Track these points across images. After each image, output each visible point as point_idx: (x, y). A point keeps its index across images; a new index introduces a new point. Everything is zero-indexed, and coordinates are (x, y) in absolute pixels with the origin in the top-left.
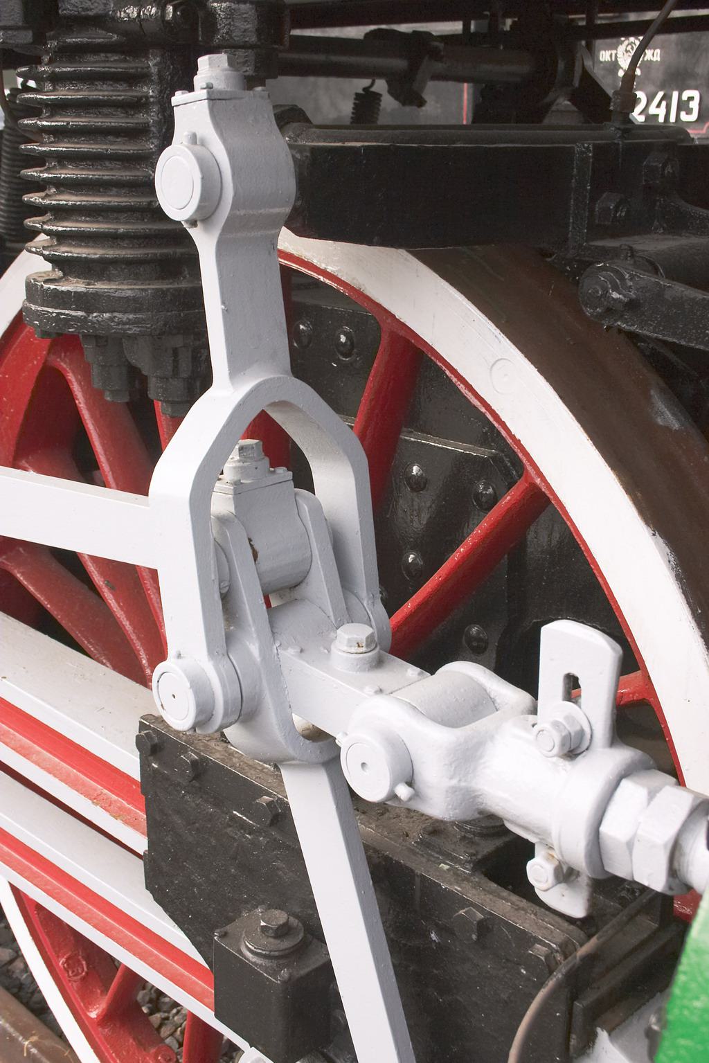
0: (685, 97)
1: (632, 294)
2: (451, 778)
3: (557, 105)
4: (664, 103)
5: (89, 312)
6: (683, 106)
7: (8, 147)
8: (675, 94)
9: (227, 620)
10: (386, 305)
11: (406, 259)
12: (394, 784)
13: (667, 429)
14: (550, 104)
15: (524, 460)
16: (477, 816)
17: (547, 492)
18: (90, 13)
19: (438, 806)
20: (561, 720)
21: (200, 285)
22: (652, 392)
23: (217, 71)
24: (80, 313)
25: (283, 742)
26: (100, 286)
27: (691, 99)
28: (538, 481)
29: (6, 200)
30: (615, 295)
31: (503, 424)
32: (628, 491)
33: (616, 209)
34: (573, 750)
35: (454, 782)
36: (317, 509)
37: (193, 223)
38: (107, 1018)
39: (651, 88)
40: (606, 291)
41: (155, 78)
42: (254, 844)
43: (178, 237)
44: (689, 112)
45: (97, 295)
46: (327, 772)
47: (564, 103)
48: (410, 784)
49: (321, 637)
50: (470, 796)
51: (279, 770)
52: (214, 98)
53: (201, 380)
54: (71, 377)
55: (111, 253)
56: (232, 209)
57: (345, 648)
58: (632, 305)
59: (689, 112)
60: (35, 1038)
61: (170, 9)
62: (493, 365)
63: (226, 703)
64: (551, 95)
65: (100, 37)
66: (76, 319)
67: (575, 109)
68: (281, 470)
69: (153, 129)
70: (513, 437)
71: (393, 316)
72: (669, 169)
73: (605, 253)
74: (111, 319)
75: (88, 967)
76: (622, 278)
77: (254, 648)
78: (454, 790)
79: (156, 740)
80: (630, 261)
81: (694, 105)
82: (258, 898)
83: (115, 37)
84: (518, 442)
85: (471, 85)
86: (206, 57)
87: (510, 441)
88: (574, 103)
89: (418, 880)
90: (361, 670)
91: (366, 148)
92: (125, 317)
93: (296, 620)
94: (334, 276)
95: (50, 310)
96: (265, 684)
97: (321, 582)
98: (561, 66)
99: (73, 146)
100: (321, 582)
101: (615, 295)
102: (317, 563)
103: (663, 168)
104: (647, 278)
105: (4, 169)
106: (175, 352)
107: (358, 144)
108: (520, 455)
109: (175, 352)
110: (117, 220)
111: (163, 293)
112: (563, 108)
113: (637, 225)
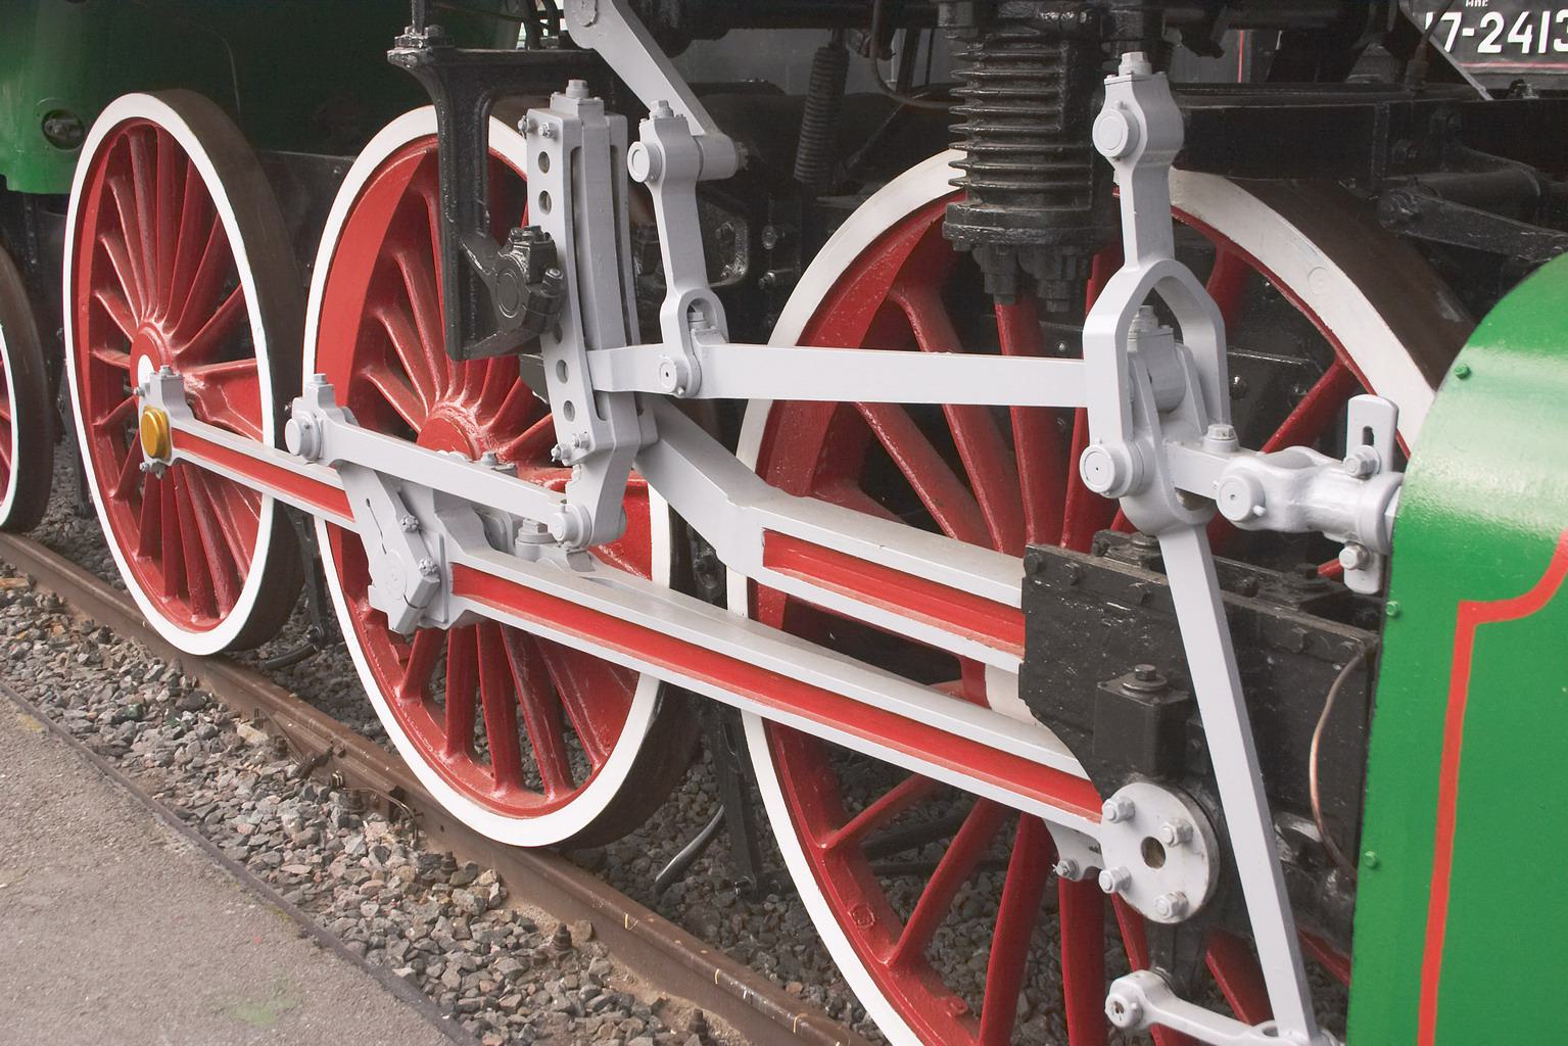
0: (1560, 18)
1: (1416, 210)
2: (1291, 499)
3: (1370, 50)
4: (1529, 28)
5: (1007, 228)
7: (812, 103)
8: (1546, 15)
9: (1134, 426)
10: (1222, 230)
11: (1240, 193)
12: (1253, 506)
13: (1451, 321)
14: (1362, 50)
15: (1335, 347)
16: (1307, 530)
17: (1354, 372)
18: (1021, 17)
19: (1281, 522)
20: (1361, 454)
22: (1439, 294)
23: (1135, 64)
24: (1000, 229)
25: (1169, 505)
26: (1012, 210)
28: (1346, 363)
29: (806, 155)
30: (1404, 211)
31: (1318, 319)
32: (1417, 363)
33: (1408, 151)
34: (1367, 473)
35: (1292, 502)
36: (1189, 355)
37: (1118, 158)
38: (900, 963)
39: (1511, 8)
40: (1396, 207)
41: (1065, 60)
42: (1126, 626)
43: (1104, 169)
45: (1014, 216)
46: (1197, 535)
47: (1376, 48)
48: (1263, 505)
49: (1195, 438)
50: (1302, 512)
51: (1157, 547)
52: (1136, 81)
53: (1115, 260)
54: (909, 309)
55: (1026, 185)
56: (1146, 149)
57: (1214, 437)
58: (1416, 218)
60: (804, 1015)
61: (1084, 15)
62: (1311, 273)
63: (1134, 475)
64: (1361, 43)
65: (1027, 32)
66: (997, 233)
67: (1387, 53)
68: (1165, 327)
69: (1062, 96)
70: (1326, 328)
71: (1227, 239)
72: (1452, 121)
73: (1398, 184)
74: (1024, 233)
75: (876, 919)
76: (1409, 199)
77: (1151, 440)
78: (1292, 507)
79: (1041, 560)
80: (1415, 187)
83: (1038, 33)
84: (1330, 332)
86: (1128, 54)
87: (1323, 333)
88: (1387, 48)
89: (1258, 618)
90: (1225, 451)
91: (1227, 110)
92: (1034, 232)
93: (1175, 429)
95: (975, 227)
96: (1157, 464)
97: (1191, 406)
98: (1373, 10)
100: (1191, 406)
101: (1404, 211)
102: (1190, 392)
103: (1448, 120)
104: (1427, 199)
105: (806, 125)
106: (1065, 259)
107: (1221, 107)
108: (1332, 344)
109: (1065, 259)
110: (1029, 162)
111: (1063, 214)
113: (1431, 166)
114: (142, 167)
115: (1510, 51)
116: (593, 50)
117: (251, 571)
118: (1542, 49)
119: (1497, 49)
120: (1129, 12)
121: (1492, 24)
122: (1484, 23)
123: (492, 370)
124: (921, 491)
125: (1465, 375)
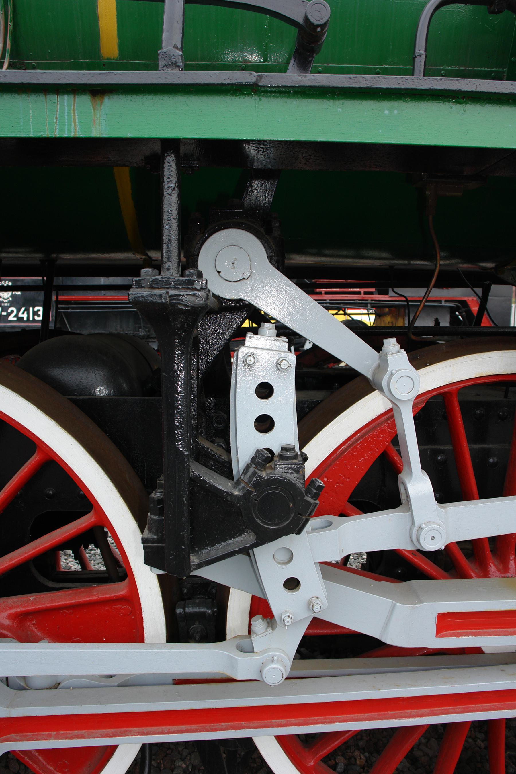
4: (26, 312)
6: (35, 313)
8: (31, 309)
21: (419, 447)
27: (39, 310)
44: (39, 316)
59: (39, 316)
81: (41, 313)
82: (204, 418)
85: (40, 326)
94: (305, 725)
99: (91, 296)
112: (446, 337)
114: (243, 94)
115: (21, 320)
116: (201, 272)
117: (314, 301)
118: (31, 319)
119: (15, 319)
120: (189, 287)
121: (12, 311)
122: (9, 311)
123: (141, 63)
124: (408, 689)
125: (457, 88)
